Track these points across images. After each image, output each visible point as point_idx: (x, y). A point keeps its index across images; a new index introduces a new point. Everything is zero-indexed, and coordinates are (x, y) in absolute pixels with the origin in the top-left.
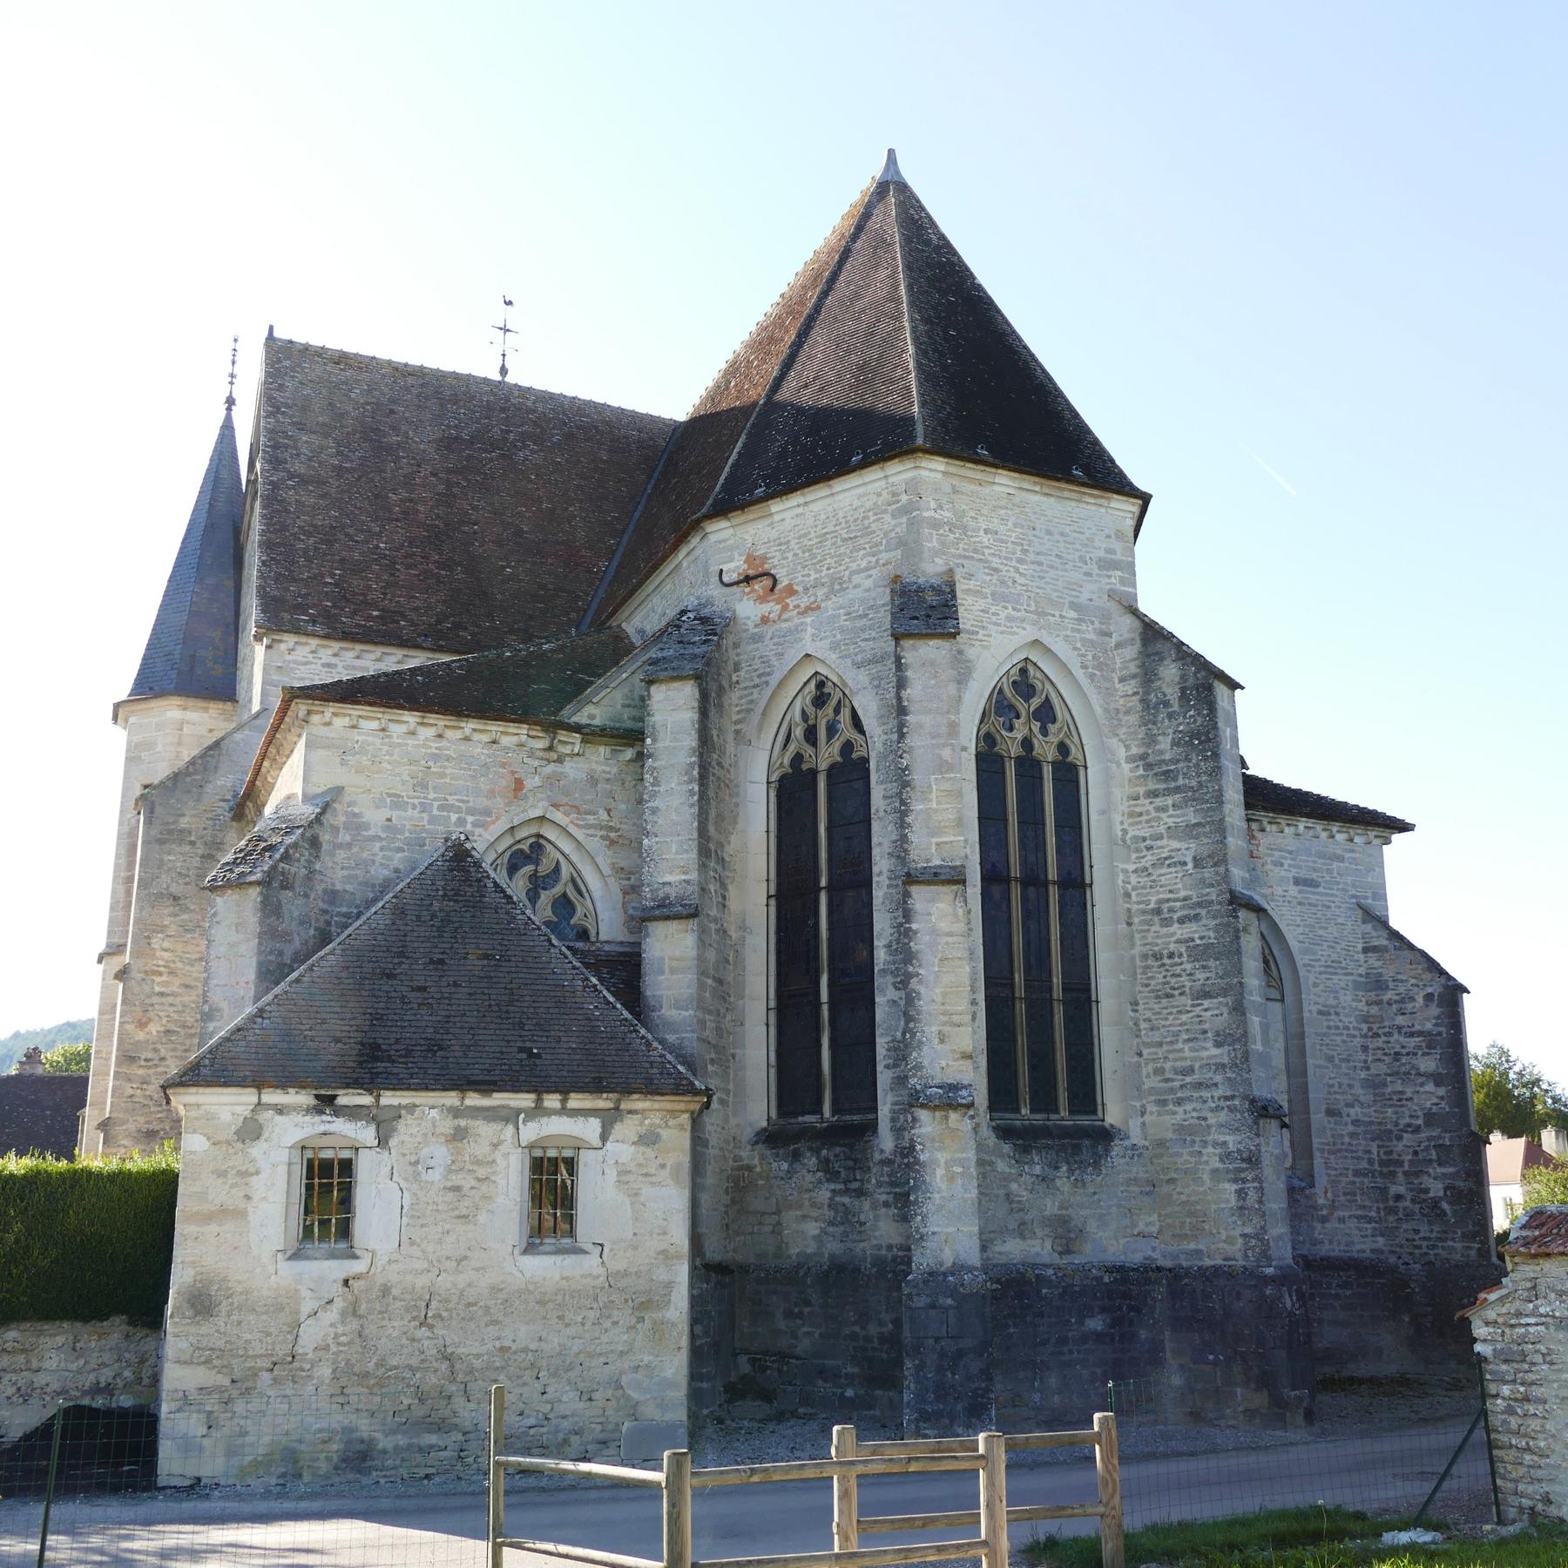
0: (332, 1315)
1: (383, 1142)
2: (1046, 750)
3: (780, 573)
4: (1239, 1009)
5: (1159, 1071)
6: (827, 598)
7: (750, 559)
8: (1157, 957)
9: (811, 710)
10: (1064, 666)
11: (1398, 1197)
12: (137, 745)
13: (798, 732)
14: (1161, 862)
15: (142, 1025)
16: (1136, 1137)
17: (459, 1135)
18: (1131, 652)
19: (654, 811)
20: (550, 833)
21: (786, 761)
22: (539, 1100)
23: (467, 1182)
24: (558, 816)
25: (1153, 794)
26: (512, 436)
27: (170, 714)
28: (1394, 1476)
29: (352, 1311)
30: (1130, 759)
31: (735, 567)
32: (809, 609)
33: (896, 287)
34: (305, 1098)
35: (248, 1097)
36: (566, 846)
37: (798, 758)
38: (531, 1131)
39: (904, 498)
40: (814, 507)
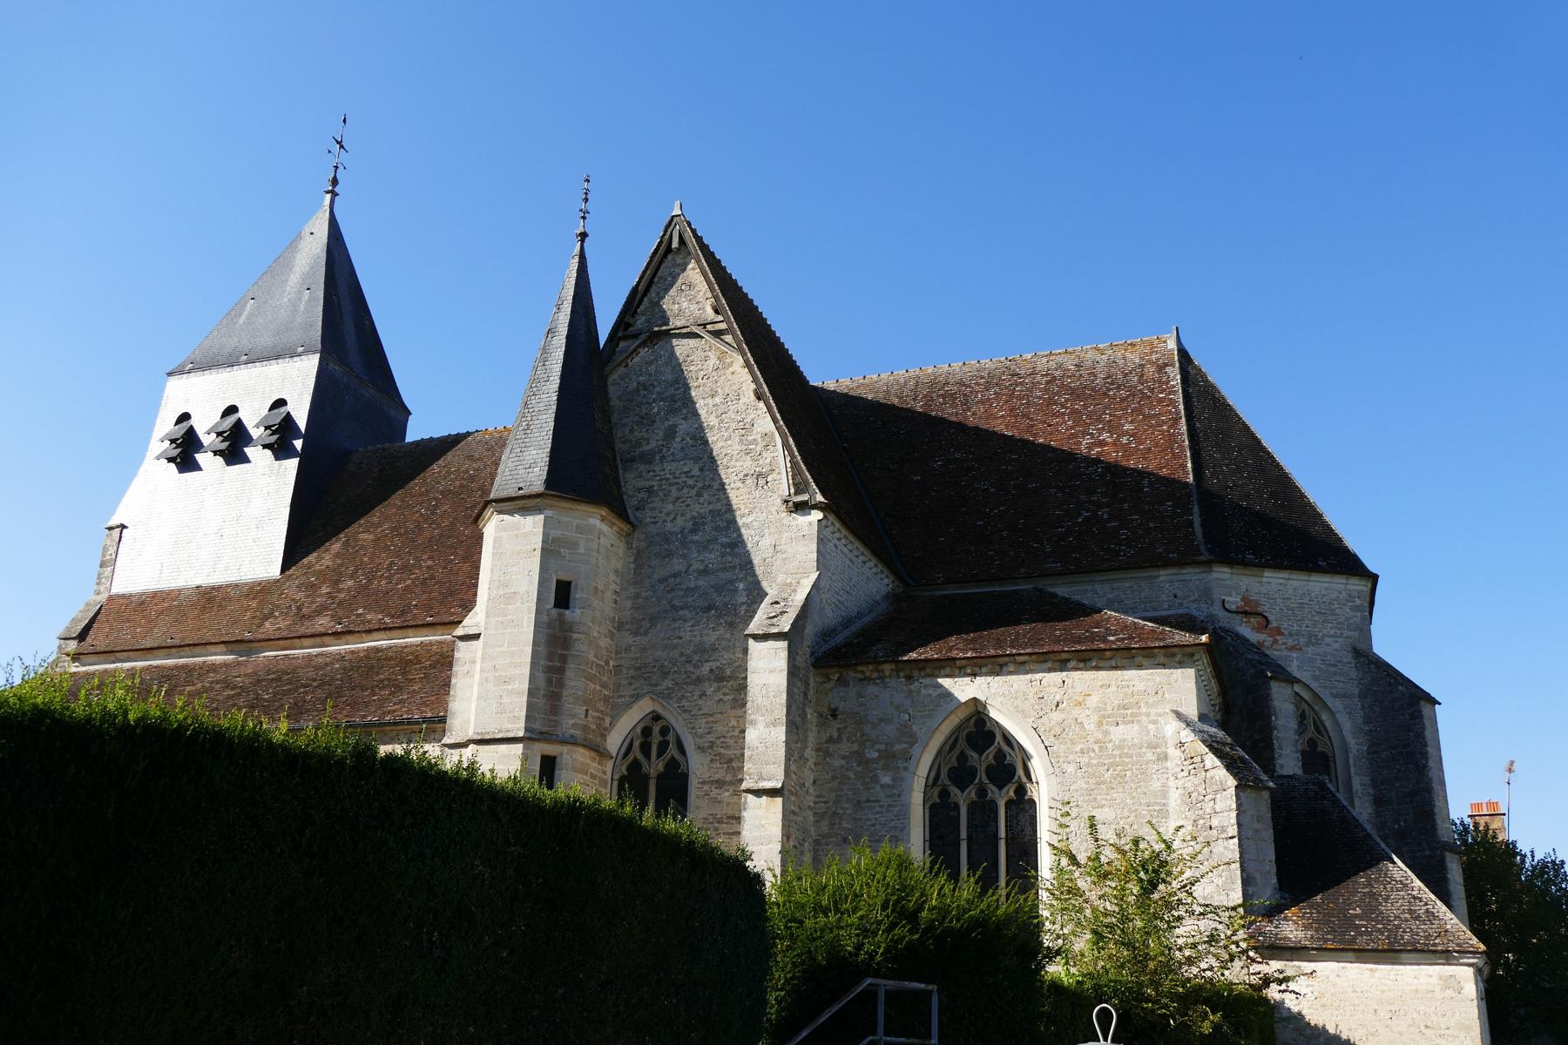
3: (1271, 618)
12: (554, 540)
31: (1234, 601)
32: (1292, 648)
40: (1296, 584)
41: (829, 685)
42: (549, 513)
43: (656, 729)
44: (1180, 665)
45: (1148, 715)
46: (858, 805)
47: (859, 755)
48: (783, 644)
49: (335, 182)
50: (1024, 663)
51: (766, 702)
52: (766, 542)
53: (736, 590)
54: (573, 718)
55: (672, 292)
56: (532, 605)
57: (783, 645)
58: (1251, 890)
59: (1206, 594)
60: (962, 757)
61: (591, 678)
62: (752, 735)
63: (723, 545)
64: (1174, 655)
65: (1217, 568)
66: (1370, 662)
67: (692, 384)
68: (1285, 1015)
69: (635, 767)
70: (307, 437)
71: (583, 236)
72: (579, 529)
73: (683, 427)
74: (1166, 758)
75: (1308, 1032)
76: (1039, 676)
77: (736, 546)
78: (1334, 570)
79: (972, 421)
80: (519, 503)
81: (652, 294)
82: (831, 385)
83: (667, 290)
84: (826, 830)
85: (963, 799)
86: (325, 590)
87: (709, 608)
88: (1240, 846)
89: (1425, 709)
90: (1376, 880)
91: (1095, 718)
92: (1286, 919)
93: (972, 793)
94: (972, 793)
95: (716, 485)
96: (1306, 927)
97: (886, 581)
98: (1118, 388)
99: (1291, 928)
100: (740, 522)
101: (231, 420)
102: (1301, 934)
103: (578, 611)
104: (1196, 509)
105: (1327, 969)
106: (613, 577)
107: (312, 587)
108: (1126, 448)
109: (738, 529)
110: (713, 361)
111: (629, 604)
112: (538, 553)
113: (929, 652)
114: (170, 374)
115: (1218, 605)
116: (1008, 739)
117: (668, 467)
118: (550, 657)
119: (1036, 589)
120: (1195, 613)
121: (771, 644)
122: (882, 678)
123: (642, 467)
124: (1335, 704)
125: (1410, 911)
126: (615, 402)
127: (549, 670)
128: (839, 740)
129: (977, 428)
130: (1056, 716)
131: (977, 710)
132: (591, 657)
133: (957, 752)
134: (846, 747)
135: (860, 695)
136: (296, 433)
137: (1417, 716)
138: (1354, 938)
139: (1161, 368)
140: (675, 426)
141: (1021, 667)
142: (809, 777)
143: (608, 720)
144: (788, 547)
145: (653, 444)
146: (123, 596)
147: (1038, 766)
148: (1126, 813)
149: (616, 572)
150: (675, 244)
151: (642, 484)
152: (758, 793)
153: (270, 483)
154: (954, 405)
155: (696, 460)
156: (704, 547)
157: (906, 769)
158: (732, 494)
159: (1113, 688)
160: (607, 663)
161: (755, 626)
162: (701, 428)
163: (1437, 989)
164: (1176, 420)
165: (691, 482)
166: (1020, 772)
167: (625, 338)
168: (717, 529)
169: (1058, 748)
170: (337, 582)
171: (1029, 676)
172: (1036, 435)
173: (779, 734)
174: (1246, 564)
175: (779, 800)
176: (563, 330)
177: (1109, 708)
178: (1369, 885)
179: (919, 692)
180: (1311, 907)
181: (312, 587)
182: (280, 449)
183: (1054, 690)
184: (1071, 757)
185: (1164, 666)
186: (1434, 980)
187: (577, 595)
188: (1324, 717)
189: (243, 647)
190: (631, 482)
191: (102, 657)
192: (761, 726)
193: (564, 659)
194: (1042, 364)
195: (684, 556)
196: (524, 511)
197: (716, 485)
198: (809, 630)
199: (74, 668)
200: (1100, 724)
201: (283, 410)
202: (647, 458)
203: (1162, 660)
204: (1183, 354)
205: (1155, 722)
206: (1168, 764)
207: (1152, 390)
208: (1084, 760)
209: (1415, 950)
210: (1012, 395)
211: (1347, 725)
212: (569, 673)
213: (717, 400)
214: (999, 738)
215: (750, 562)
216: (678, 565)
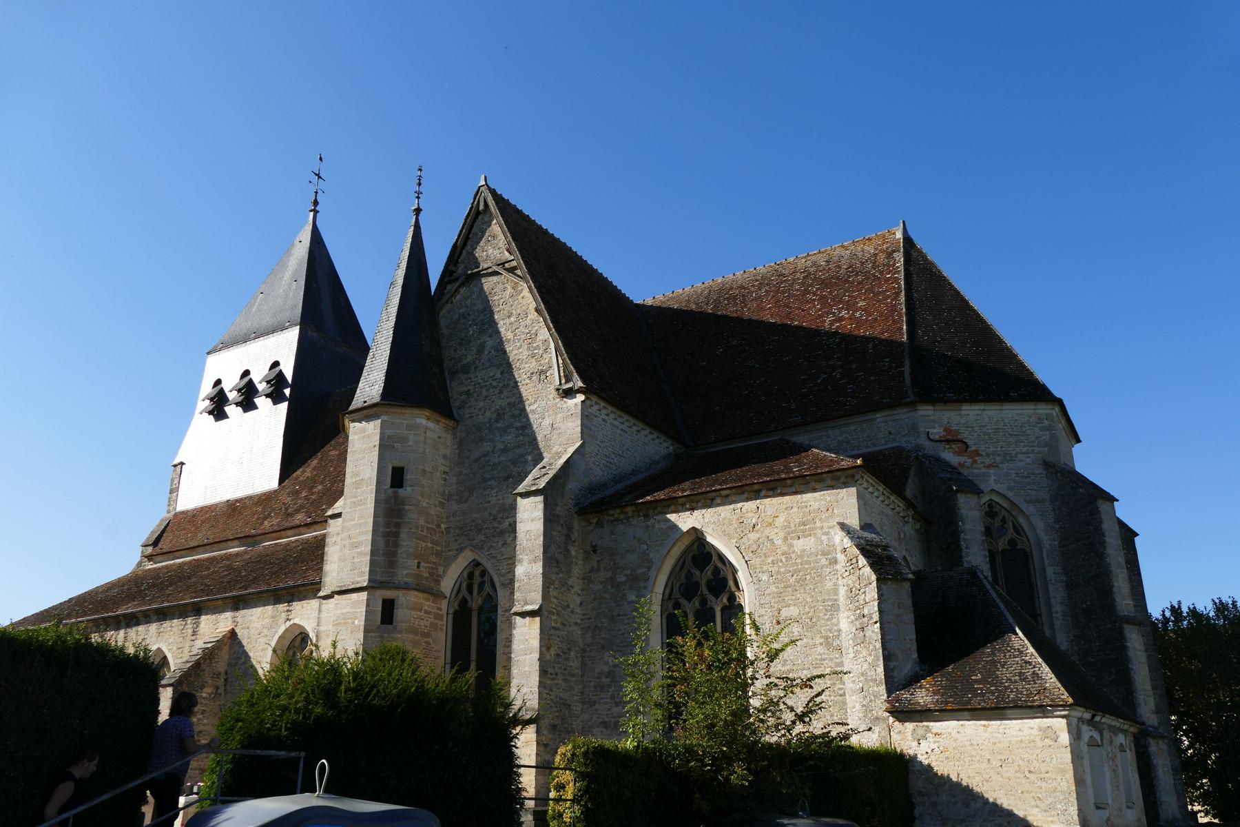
3: (970, 443)
6: (1003, 462)
7: (946, 430)
12: (389, 437)
15: (548, 649)
21: (683, 577)
22: (1093, 716)
27: (418, 420)
28: (217, 688)
31: (937, 432)
32: (990, 466)
39: (1046, 422)
40: (990, 413)
41: (591, 528)
42: (385, 418)
43: (477, 573)
44: (845, 485)
45: (822, 528)
47: (612, 579)
48: (540, 499)
49: (316, 203)
50: (727, 496)
51: (530, 544)
52: (547, 422)
53: (526, 462)
54: (407, 569)
55: (482, 243)
56: (373, 487)
57: (540, 499)
58: (892, 665)
59: (914, 429)
60: (690, 575)
61: (423, 539)
62: (520, 571)
63: (517, 429)
64: (839, 478)
65: (921, 407)
66: (1057, 472)
67: (496, 310)
68: (918, 768)
69: (463, 602)
70: (292, 386)
71: (418, 211)
72: (409, 428)
73: (490, 343)
74: (836, 561)
75: (936, 781)
76: (740, 505)
77: (526, 428)
78: (1023, 399)
79: (747, 315)
80: (367, 412)
81: (468, 247)
82: (649, 302)
83: (478, 242)
84: (589, 640)
86: (304, 494)
87: (507, 478)
88: (881, 628)
89: (1103, 506)
90: (1000, 650)
91: (781, 534)
92: (921, 687)
93: (696, 603)
94: (696, 603)
95: (512, 384)
96: (935, 693)
97: (665, 444)
98: (857, 275)
99: (923, 696)
100: (528, 409)
101: (246, 380)
102: (929, 699)
103: (409, 489)
104: (907, 362)
105: (948, 727)
106: (441, 461)
107: (297, 493)
108: (859, 322)
109: (527, 416)
110: (509, 290)
111: (454, 480)
112: (377, 449)
113: (661, 495)
114: (208, 353)
115: (923, 436)
116: (722, 558)
117: (480, 374)
118: (388, 525)
119: (781, 439)
120: (904, 445)
121: (532, 499)
122: (627, 518)
123: (462, 377)
124: (1029, 509)
125: (1020, 674)
126: (445, 331)
127: (387, 535)
128: (598, 570)
129: (750, 320)
130: (753, 536)
131: (697, 536)
132: (422, 522)
133: (684, 572)
134: (603, 575)
135: (612, 533)
136: (286, 384)
137: (1095, 512)
138: (970, 699)
139: (890, 255)
140: (484, 343)
141: (726, 501)
142: (574, 600)
143: (441, 570)
144: (559, 421)
145: (470, 358)
146: (183, 513)
147: (742, 576)
148: (807, 609)
149: (445, 457)
150: (481, 208)
151: (462, 389)
152: (523, 615)
153: (271, 419)
154: (735, 304)
156: (504, 431)
157: (645, 588)
158: (523, 389)
159: (795, 510)
160: (439, 526)
161: (521, 488)
162: (501, 342)
163: (1038, 739)
164: (898, 294)
165: (495, 383)
166: (731, 583)
167: (450, 282)
168: (514, 416)
169: (755, 561)
170: (313, 487)
171: (732, 506)
172: (792, 320)
173: (538, 568)
174: (945, 401)
175: (538, 619)
176: (400, 281)
177: (792, 525)
178: (993, 654)
179: (653, 526)
180: (943, 676)
181: (297, 493)
182: (276, 397)
183: (750, 515)
184: (765, 568)
185: (833, 487)
186: (1035, 732)
187: (408, 477)
188: (1021, 520)
189: (250, 540)
190: (456, 389)
191: (166, 556)
192: (525, 563)
193: (398, 525)
194: (801, 264)
195: (491, 440)
196: (368, 418)
197: (512, 384)
198: (572, 486)
199: (150, 566)
200: (786, 539)
201: (277, 369)
202: (466, 369)
203: (830, 482)
204: (908, 240)
205: (827, 534)
206: (838, 567)
207: (881, 273)
208: (775, 569)
209: (1016, 707)
210: (777, 292)
211: (1040, 525)
212: (403, 536)
213: (512, 319)
214: (715, 558)
215: (535, 439)
216: (487, 447)
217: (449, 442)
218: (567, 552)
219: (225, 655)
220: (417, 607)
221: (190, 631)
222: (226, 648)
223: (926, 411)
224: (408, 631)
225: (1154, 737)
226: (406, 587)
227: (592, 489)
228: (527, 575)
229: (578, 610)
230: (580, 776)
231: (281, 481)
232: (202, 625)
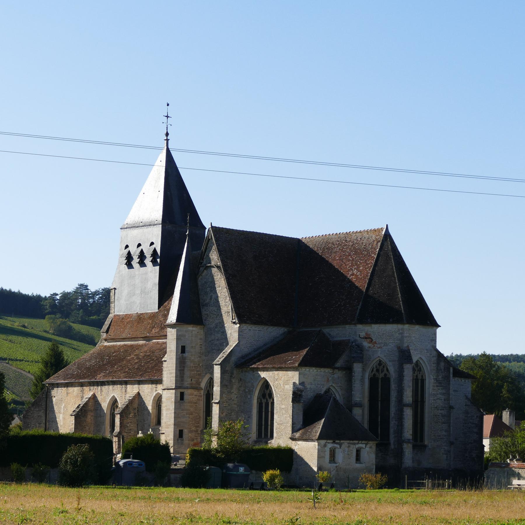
0: (335, 471)
1: (340, 448)
2: (420, 377)
3: (373, 339)
4: (449, 426)
5: (434, 436)
6: (384, 346)
7: (366, 334)
8: (436, 416)
9: (378, 367)
10: (424, 362)
11: (467, 457)
12: (180, 335)
13: (375, 370)
14: (438, 399)
15: (222, 413)
16: (430, 447)
17: (349, 447)
18: (435, 358)
19: (354, 387)
20: (331, 388)
23: (349, 453)
24: (334, 385)
25: (437, 386)
26: (266, 253)
27: (189, 328)
29: (337, 471)
30: (434, 379)
31: (363, 334)
32: (379, 348)
33: (394, 274)
34: (331, 441)
35: (325, 441)
36: (333, 390)
37: (374, 375)
38: (357, 446)
42: (178, 328)
46: (244, 403)
47: (244, 390)
48: (219, 366)
54: (187, 382)
62: (215, 389)
72: (186, 331)
73: (213, 296)
81: (207, 253)
83: (210, 251)
85: (264, 401)
99: (297, 435)
103: (187, 354)
117: (211, 308)
118: (180, 367)
126: (200, 287)
127: (180, 370)
130: (277, 382)
134: (242, 389)
142: (234, 396)
143: (200, 380)
149: (201, 339)
155: (216, 306)
160: (199, 365)
161: (214, 363)
168: (220, 327)
173: (219, 389)
187: (186, 349)
193: (184, 367)
217: (202, 333)
218: (231, 381)
219: (136, 401)
220: (192, 394)
221: (124, 390)
222: (137, 399)
223: (360, 326)
224: (189, 403)
225: (406, 443)
226: (187, 388)
227: (243, 357)
228: (216, 390)
229: (236, 399)
230: (190, 455)
231: (159, 307)
232: (128, 389)
